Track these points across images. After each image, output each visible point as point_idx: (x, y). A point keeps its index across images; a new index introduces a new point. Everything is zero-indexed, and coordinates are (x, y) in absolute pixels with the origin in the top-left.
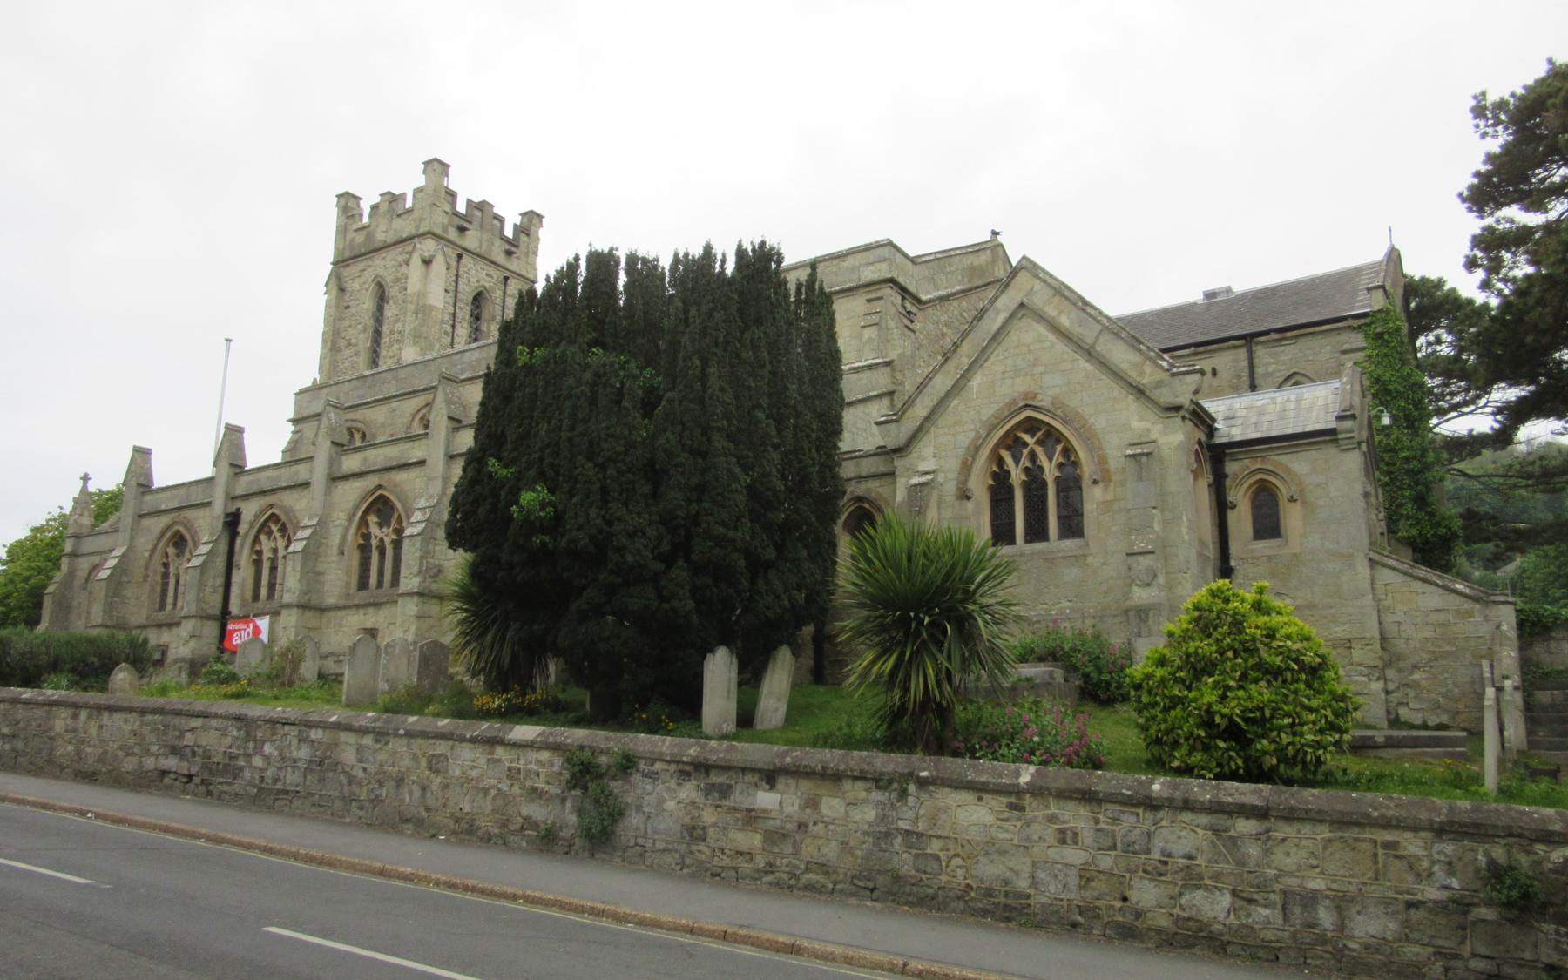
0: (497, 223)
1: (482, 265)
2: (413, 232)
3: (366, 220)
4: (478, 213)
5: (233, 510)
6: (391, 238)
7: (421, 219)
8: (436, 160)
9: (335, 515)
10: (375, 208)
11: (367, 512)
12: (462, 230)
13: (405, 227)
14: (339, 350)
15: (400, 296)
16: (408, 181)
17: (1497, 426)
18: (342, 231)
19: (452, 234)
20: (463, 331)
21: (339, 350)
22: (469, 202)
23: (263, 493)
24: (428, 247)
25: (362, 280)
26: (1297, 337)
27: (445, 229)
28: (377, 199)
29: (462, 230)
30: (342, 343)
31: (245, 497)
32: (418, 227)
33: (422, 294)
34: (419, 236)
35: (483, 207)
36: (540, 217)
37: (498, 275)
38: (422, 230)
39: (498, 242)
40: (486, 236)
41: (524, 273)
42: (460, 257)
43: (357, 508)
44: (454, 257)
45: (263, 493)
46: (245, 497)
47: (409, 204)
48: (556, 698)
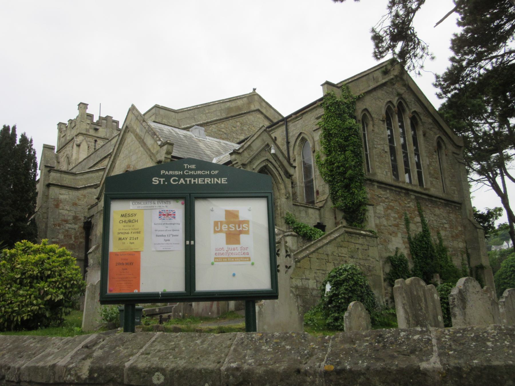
0: (115, 124)
8: (81, 103)
12: (96, 130)
17: (469, 176)
19: (92, 132)
26: (276, 128)
29: (96, 130)
35: (107, 118)
42: (96, 141)
44: (93, 141)
48: (394, 16)
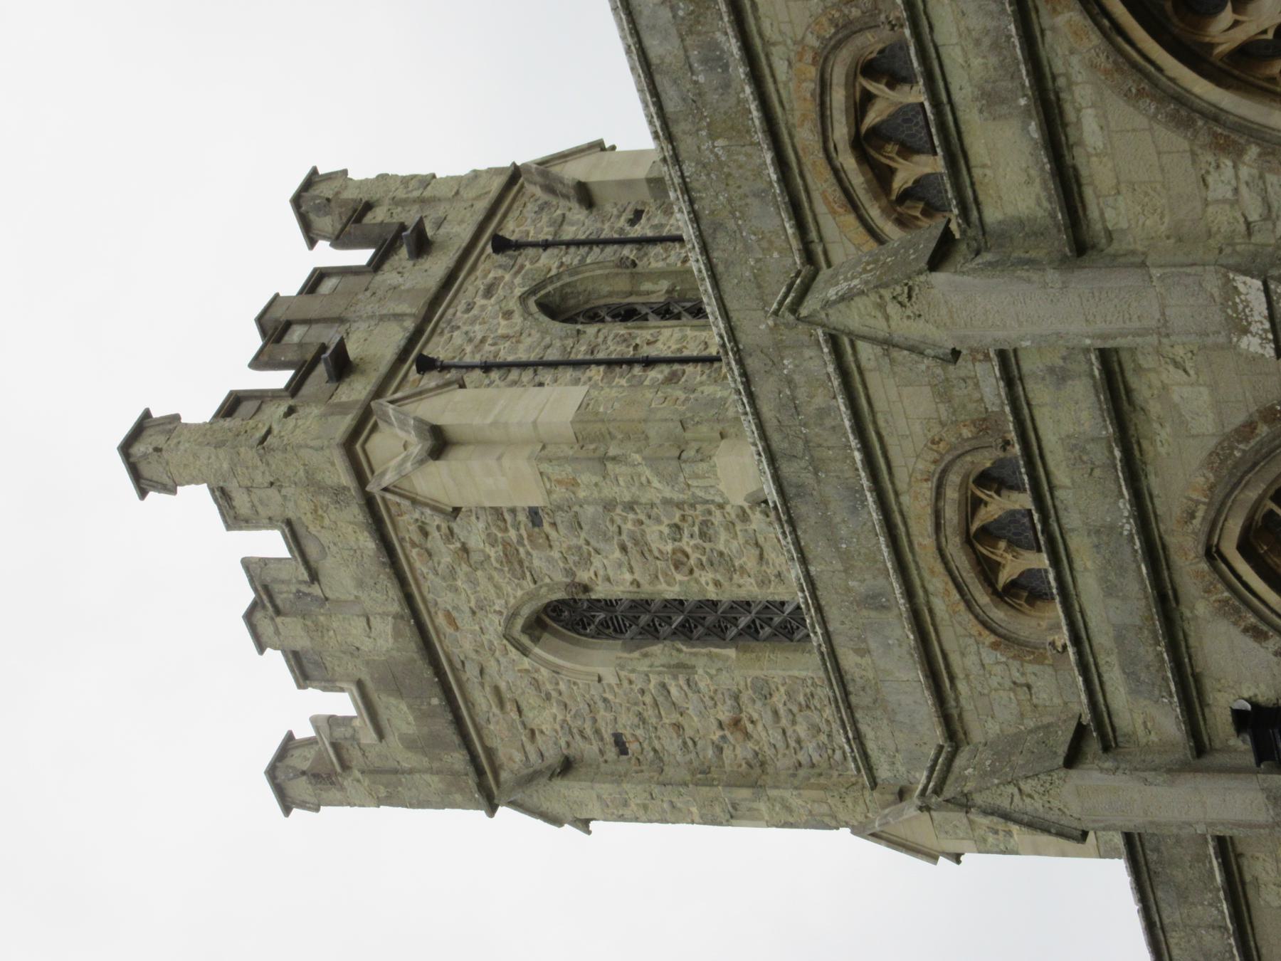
0: (328, 285)
1: (456, 310)
2: (355, 511)
3: (342, 704)
4: (296, 334)
5: (1242, 746)
6: (387, 600)
7: (313, 484)
8: (126, 448)
9: (1223, 219)
10: (306, 671)
11: (1196, 58)
13: (345, 537)
14: (760, 763)
15: (562, 538)
16: (201, 551)
18: (390, 788)
19: (356, 390)
20: (668, 338)
21: (760, 763)
22: (260, 362)
23: (1166, 602)
24: (392, 448)
25: (530, 700)
27: (343, 408)
28: (275, 659)
30: (738, 752)
31: (1189, 689)
32: (338, 493)
33: (544, 449)
34: (361, 479)
35: (275, 326)
36: (312, 179)
37: (490, 266)
38: (344, 478)
39: (388, 276)
40: (367, 306)
41: (483, 205)
43: (1184, 111)
45: (1166, 602)
46: (1189, 689)
47: (271, 544)
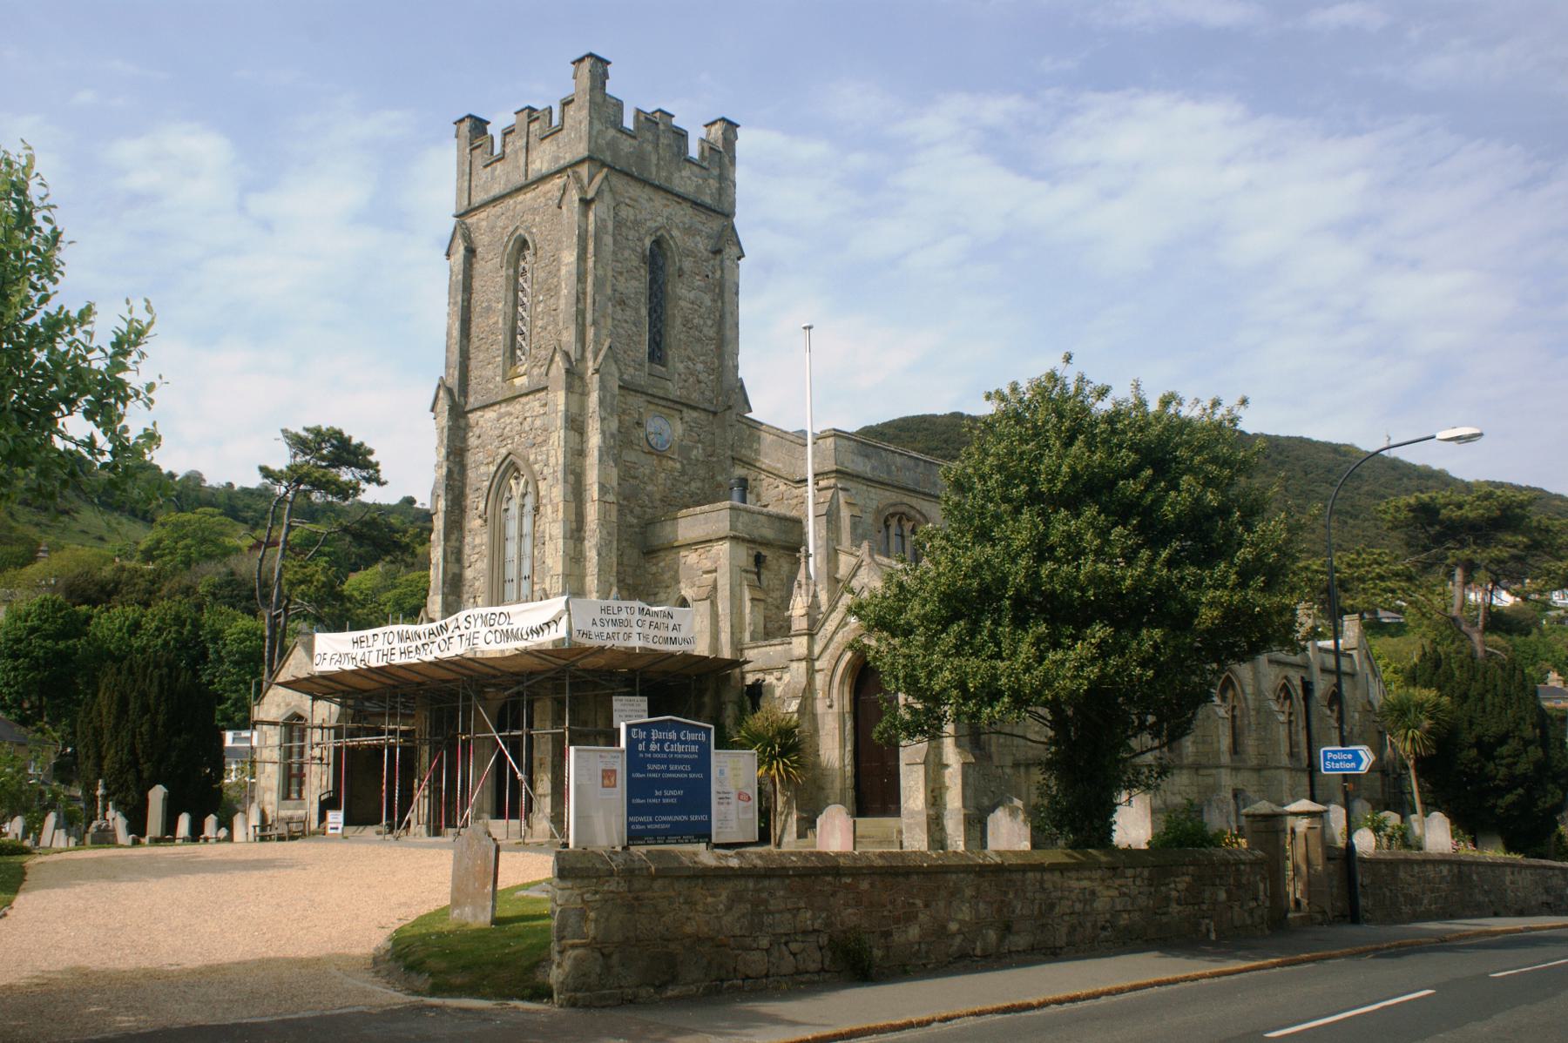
22: (639, 111)
